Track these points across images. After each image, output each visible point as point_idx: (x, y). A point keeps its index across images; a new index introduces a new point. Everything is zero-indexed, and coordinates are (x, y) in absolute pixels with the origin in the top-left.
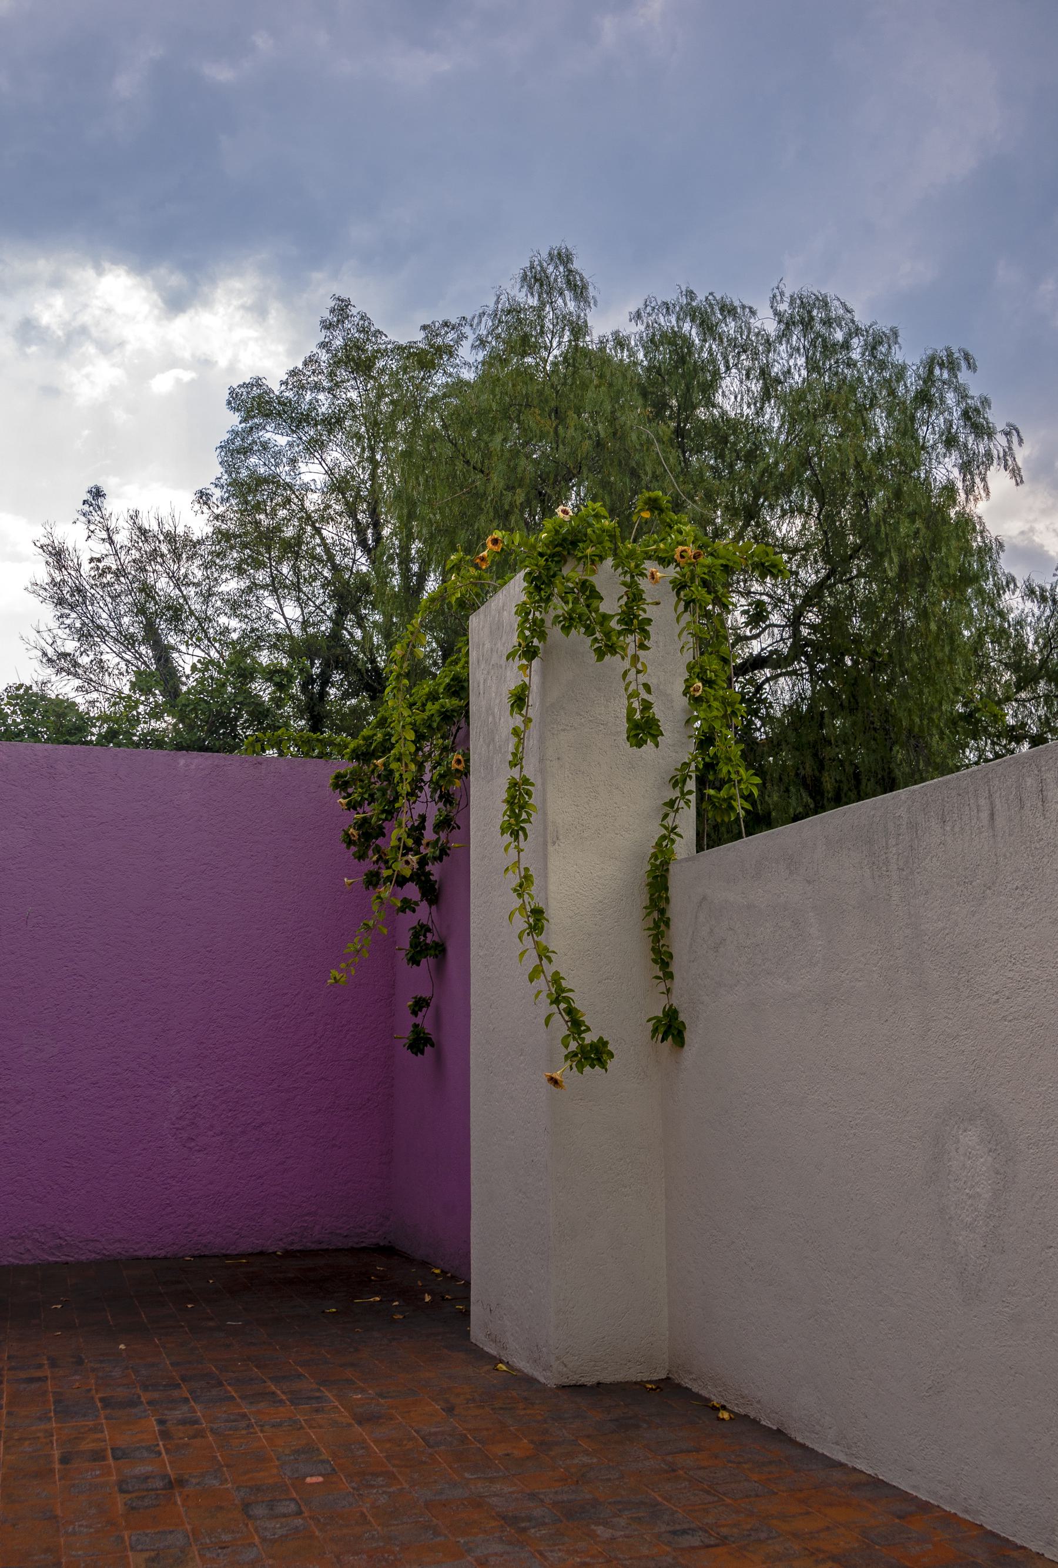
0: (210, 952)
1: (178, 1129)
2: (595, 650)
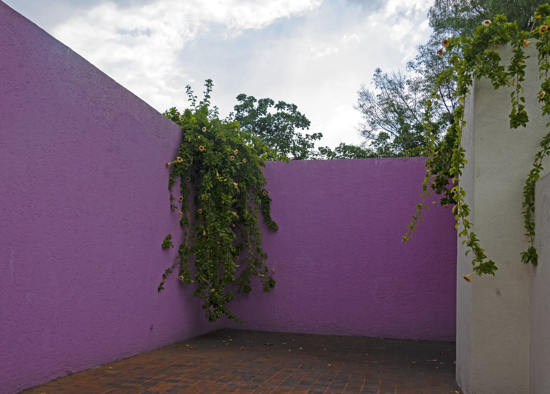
0: (388, 231)
1: (378, 294)
2: (494, 84)
